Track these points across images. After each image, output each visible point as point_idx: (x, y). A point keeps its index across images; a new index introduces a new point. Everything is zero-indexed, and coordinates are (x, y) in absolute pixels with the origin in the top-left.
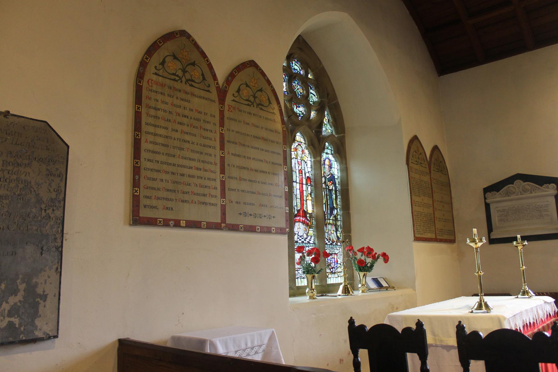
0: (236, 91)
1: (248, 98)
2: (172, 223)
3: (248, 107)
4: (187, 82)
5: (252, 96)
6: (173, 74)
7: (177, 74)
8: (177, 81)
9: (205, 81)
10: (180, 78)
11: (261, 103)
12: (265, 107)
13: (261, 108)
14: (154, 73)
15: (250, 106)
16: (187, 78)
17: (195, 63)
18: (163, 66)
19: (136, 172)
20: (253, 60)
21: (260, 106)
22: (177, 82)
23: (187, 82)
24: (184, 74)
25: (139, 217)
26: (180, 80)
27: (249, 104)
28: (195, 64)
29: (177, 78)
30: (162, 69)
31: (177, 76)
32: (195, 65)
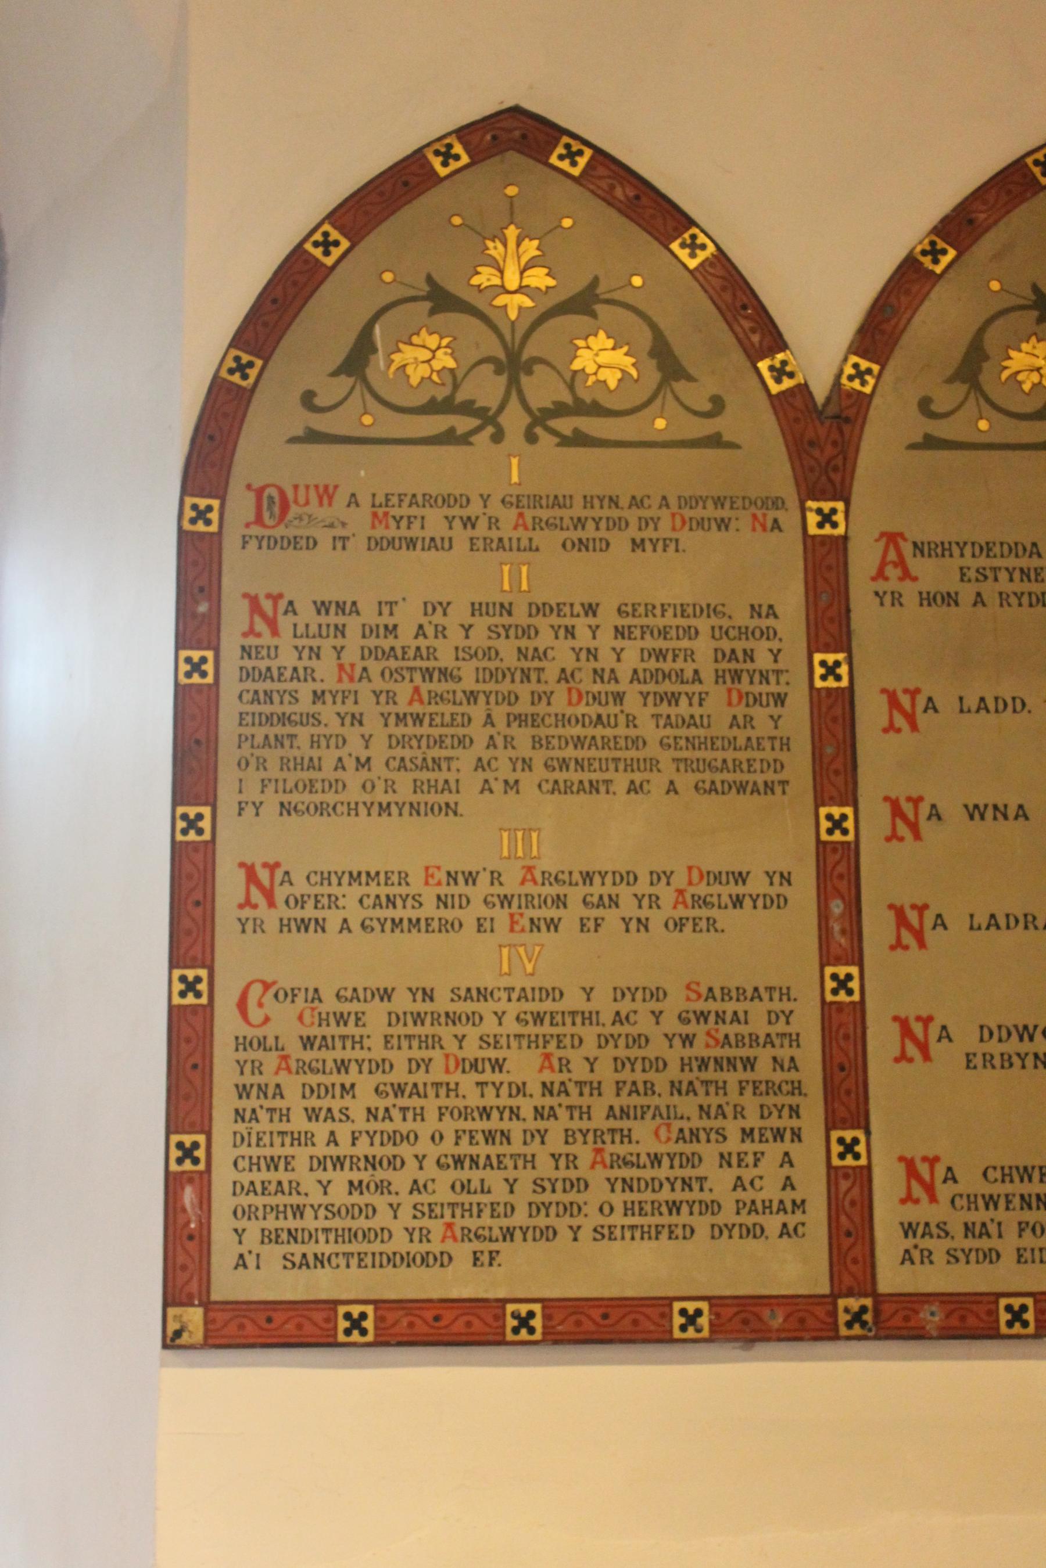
0: (949, 372)
1: (446, 391)
2: (932, 1317)
3: (452, 450)
4: (539, 430)
5: (489, 368)
6: (432, 407)
7: (460, 397)
8: (465, 440)
9: (680, 386)
10: (488, 418)
11: (577, 399)
12: (944, 422)
13: (576, 431)
14: (300, 432)
15: (470, 444)
16: (535, 404)
17: (598, 291)
18: (976, 386)
19: (846, 1037)
20: (516, 111)
21: (565, 425)
22: (465, 448)
23: (539, 430)
24: (514, 382)
25: (874, 1294)
26: (490, 430)
27: (452, 430)
28: (597, 299)
29: (464, 424)
30: (972, 395)
31: (467, 408)
32: (599, 308)
